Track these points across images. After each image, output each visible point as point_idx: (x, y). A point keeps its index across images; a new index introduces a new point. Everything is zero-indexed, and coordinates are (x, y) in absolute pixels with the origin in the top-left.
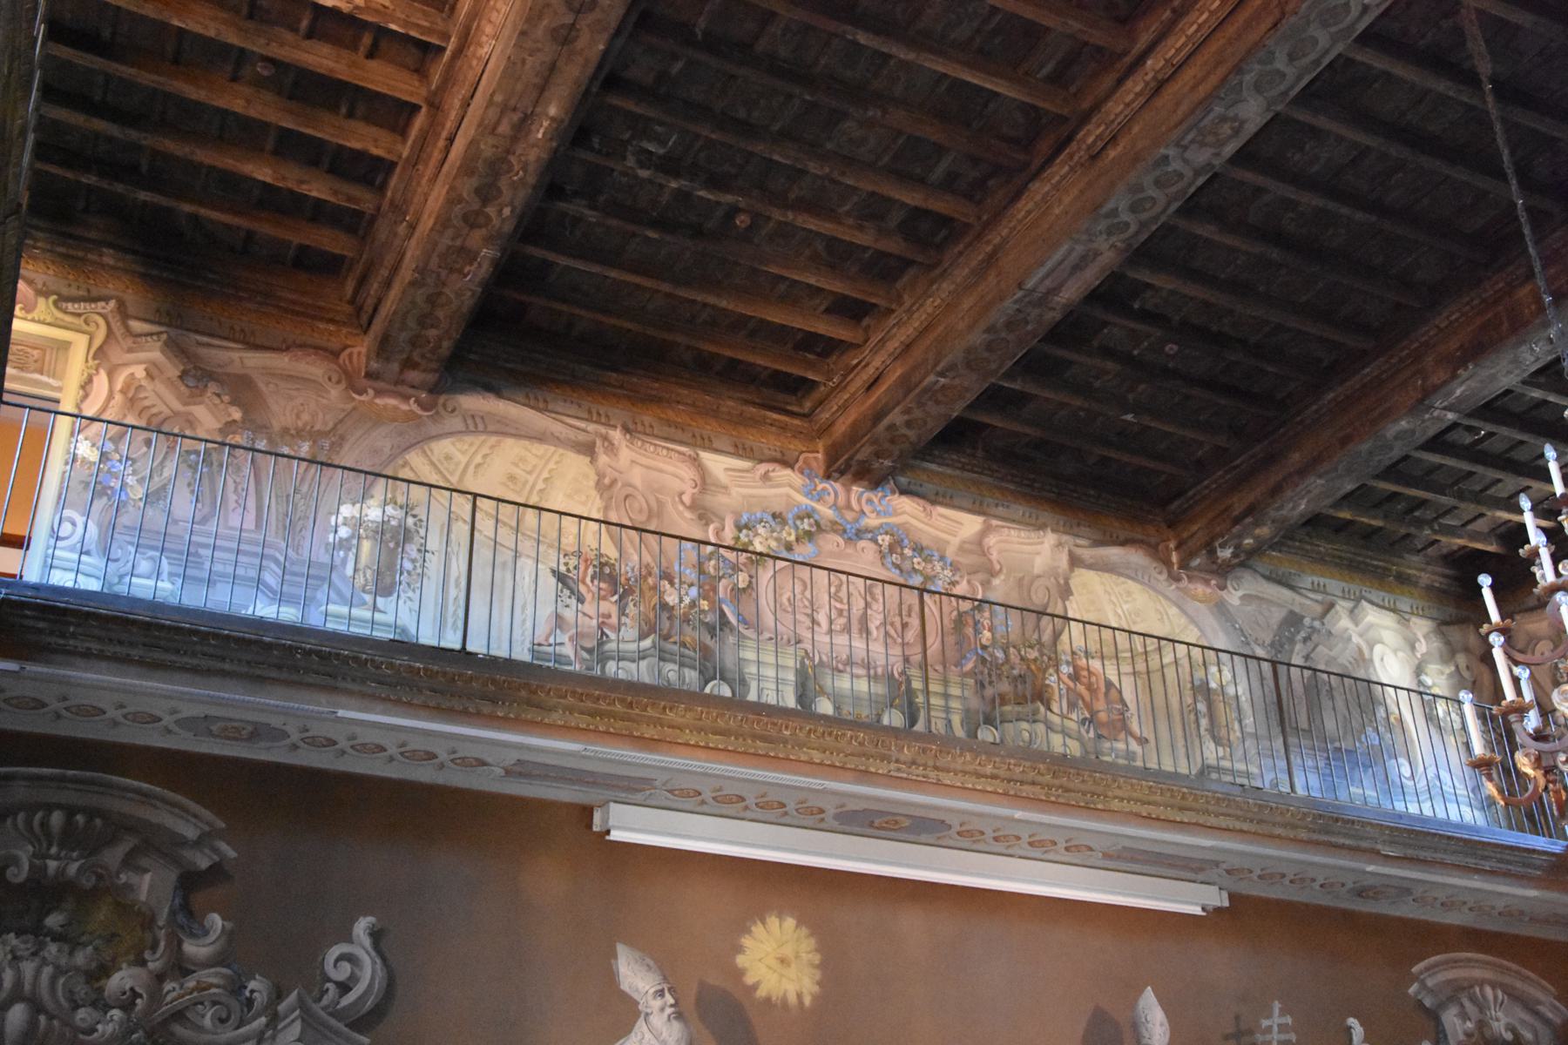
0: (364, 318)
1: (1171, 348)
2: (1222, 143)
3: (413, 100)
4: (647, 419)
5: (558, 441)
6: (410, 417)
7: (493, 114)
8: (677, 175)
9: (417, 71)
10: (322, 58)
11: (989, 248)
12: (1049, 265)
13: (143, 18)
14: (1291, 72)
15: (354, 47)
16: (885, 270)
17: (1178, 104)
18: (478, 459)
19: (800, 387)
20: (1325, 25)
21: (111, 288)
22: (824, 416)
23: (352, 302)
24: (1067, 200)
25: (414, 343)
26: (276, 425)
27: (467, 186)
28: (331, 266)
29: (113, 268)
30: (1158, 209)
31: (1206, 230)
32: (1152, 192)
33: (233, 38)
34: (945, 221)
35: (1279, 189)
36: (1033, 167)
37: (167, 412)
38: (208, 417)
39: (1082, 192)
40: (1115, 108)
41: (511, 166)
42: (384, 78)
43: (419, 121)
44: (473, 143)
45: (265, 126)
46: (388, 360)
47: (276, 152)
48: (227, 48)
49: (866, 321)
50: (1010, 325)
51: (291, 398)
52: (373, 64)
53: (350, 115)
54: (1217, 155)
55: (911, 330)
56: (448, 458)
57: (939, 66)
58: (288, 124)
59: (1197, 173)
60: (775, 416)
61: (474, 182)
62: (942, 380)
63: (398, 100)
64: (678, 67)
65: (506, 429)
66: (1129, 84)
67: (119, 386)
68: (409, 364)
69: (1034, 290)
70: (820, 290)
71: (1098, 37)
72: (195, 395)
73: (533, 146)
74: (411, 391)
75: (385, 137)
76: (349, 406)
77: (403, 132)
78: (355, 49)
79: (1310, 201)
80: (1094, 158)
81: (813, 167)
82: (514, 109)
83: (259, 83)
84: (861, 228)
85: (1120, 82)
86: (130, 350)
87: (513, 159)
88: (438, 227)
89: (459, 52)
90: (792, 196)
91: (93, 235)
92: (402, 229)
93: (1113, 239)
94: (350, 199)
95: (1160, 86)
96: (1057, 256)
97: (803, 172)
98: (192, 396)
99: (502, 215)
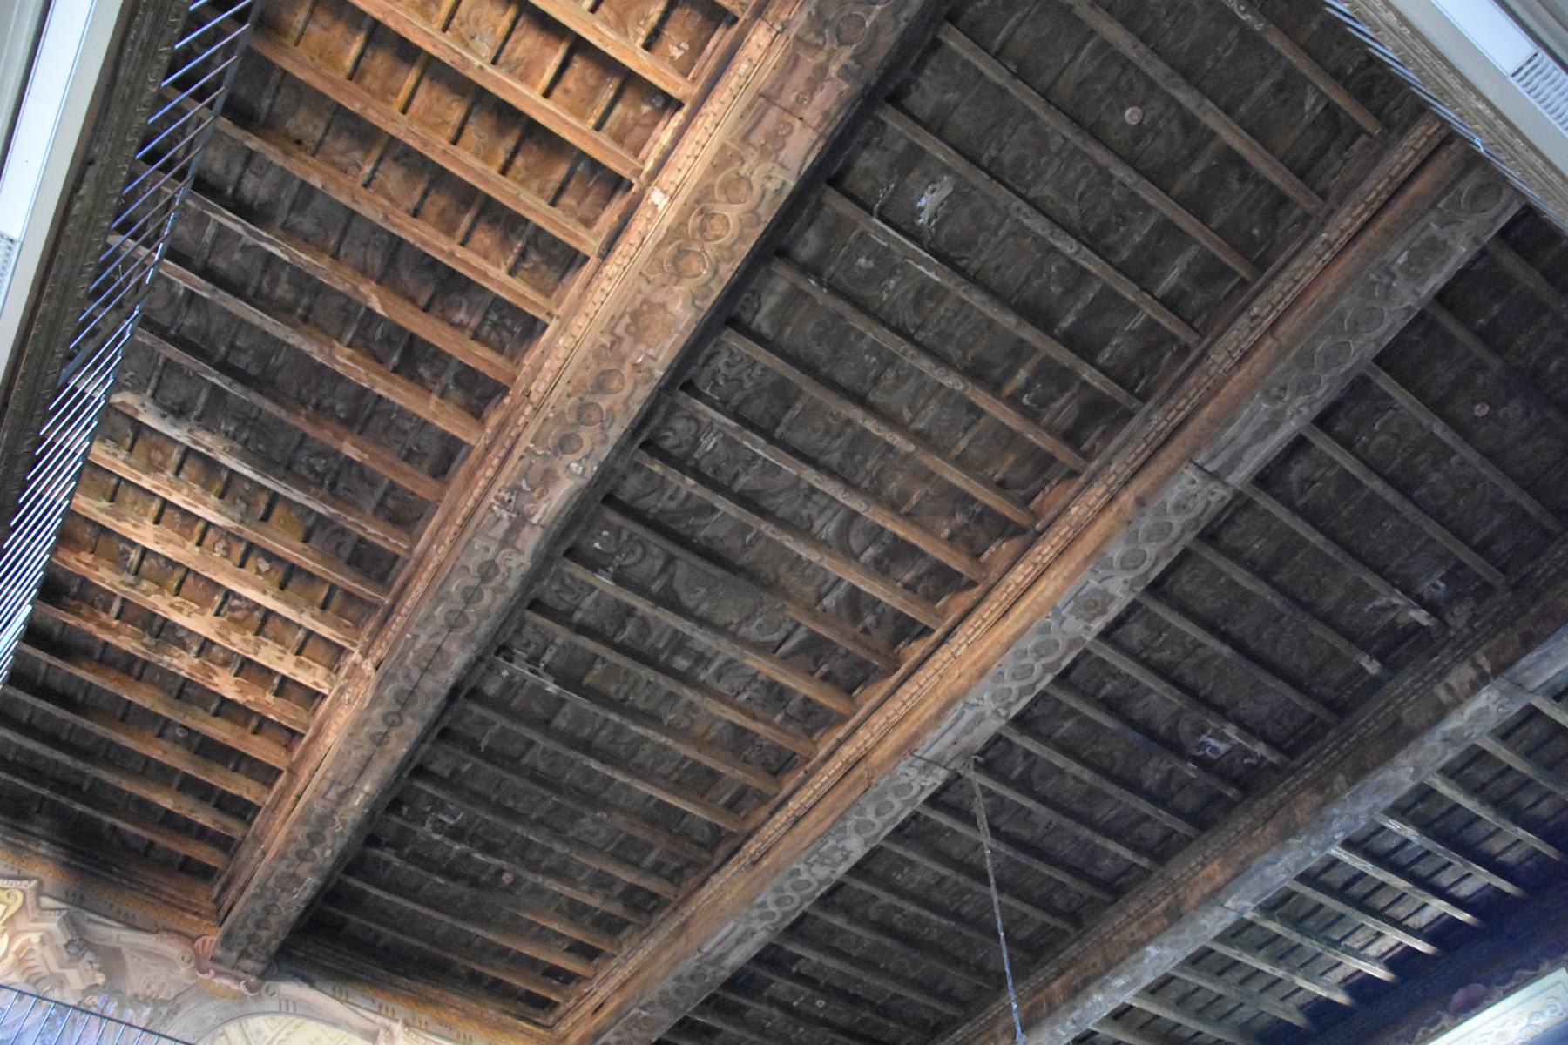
0: (222, 914)
1: (820, 1003)
2: (835, 865)
3: (279, 766)
4: (424, 1018)
5: (350, 1028)
6: (239, 997)
7: (324, 785)
10: (220, 731)
11: (683, 919)
13: (105, 691)
14: (878, 823)
15: (245, 724)
16: (611, 926)
18: (282, 1036)
19: (546, 1004)
20: (897, 794)
21: (38, 871)
22: (562, 1029)
23: (216, 901)
24: (735, 891)
25: (251, 938)
26: (129, 993)
27: (301, 833)
28: (206, 873)
29: (45, 856)
30: (795, 905)
31: (838, 921)
32: (789, 893)
33: (161, 710)
34: (654, 896)
35: (886, 898)
37: (45, 972)
38: (78, 979)
40: (768, 832)
42: (261, 749)
43: (281, 781)
45: (175, 771)
46: (229, 949)
47: (179, 789)
48: (156, 717)
49: (596, 961)
51: (147, 970)
52: (257, 738)
53: (235, 770)
56: (259, 1032)
58: (190, 771)
60: (525, 1025)
61: (307, 829)
62: (644, 1013)
64: (466, 768)
65: (310, 1013)
66: (777, 816)
67: (15, 947)
68: (244, 955)
69: (708, 954)
70: (563, 935)
71: (755, 783)
72: (74, 960)
74: (241, 974)
76: (192, 982)
77: (271, 786)
79: (912, 908)
80: (754, 863)
81: (558, 847)
83: (176, 741)
84: (591, 893)
85: (772, 814)
86: (35, 920)
87: (336, 818)
89: (314, 739)
90: (543, 865)
91: (36, 830)
92: (257, 854)
94: (225, 828)
95: (797, 821)
97: (551, 851)
98: (71, 961)
99: (326, 854)
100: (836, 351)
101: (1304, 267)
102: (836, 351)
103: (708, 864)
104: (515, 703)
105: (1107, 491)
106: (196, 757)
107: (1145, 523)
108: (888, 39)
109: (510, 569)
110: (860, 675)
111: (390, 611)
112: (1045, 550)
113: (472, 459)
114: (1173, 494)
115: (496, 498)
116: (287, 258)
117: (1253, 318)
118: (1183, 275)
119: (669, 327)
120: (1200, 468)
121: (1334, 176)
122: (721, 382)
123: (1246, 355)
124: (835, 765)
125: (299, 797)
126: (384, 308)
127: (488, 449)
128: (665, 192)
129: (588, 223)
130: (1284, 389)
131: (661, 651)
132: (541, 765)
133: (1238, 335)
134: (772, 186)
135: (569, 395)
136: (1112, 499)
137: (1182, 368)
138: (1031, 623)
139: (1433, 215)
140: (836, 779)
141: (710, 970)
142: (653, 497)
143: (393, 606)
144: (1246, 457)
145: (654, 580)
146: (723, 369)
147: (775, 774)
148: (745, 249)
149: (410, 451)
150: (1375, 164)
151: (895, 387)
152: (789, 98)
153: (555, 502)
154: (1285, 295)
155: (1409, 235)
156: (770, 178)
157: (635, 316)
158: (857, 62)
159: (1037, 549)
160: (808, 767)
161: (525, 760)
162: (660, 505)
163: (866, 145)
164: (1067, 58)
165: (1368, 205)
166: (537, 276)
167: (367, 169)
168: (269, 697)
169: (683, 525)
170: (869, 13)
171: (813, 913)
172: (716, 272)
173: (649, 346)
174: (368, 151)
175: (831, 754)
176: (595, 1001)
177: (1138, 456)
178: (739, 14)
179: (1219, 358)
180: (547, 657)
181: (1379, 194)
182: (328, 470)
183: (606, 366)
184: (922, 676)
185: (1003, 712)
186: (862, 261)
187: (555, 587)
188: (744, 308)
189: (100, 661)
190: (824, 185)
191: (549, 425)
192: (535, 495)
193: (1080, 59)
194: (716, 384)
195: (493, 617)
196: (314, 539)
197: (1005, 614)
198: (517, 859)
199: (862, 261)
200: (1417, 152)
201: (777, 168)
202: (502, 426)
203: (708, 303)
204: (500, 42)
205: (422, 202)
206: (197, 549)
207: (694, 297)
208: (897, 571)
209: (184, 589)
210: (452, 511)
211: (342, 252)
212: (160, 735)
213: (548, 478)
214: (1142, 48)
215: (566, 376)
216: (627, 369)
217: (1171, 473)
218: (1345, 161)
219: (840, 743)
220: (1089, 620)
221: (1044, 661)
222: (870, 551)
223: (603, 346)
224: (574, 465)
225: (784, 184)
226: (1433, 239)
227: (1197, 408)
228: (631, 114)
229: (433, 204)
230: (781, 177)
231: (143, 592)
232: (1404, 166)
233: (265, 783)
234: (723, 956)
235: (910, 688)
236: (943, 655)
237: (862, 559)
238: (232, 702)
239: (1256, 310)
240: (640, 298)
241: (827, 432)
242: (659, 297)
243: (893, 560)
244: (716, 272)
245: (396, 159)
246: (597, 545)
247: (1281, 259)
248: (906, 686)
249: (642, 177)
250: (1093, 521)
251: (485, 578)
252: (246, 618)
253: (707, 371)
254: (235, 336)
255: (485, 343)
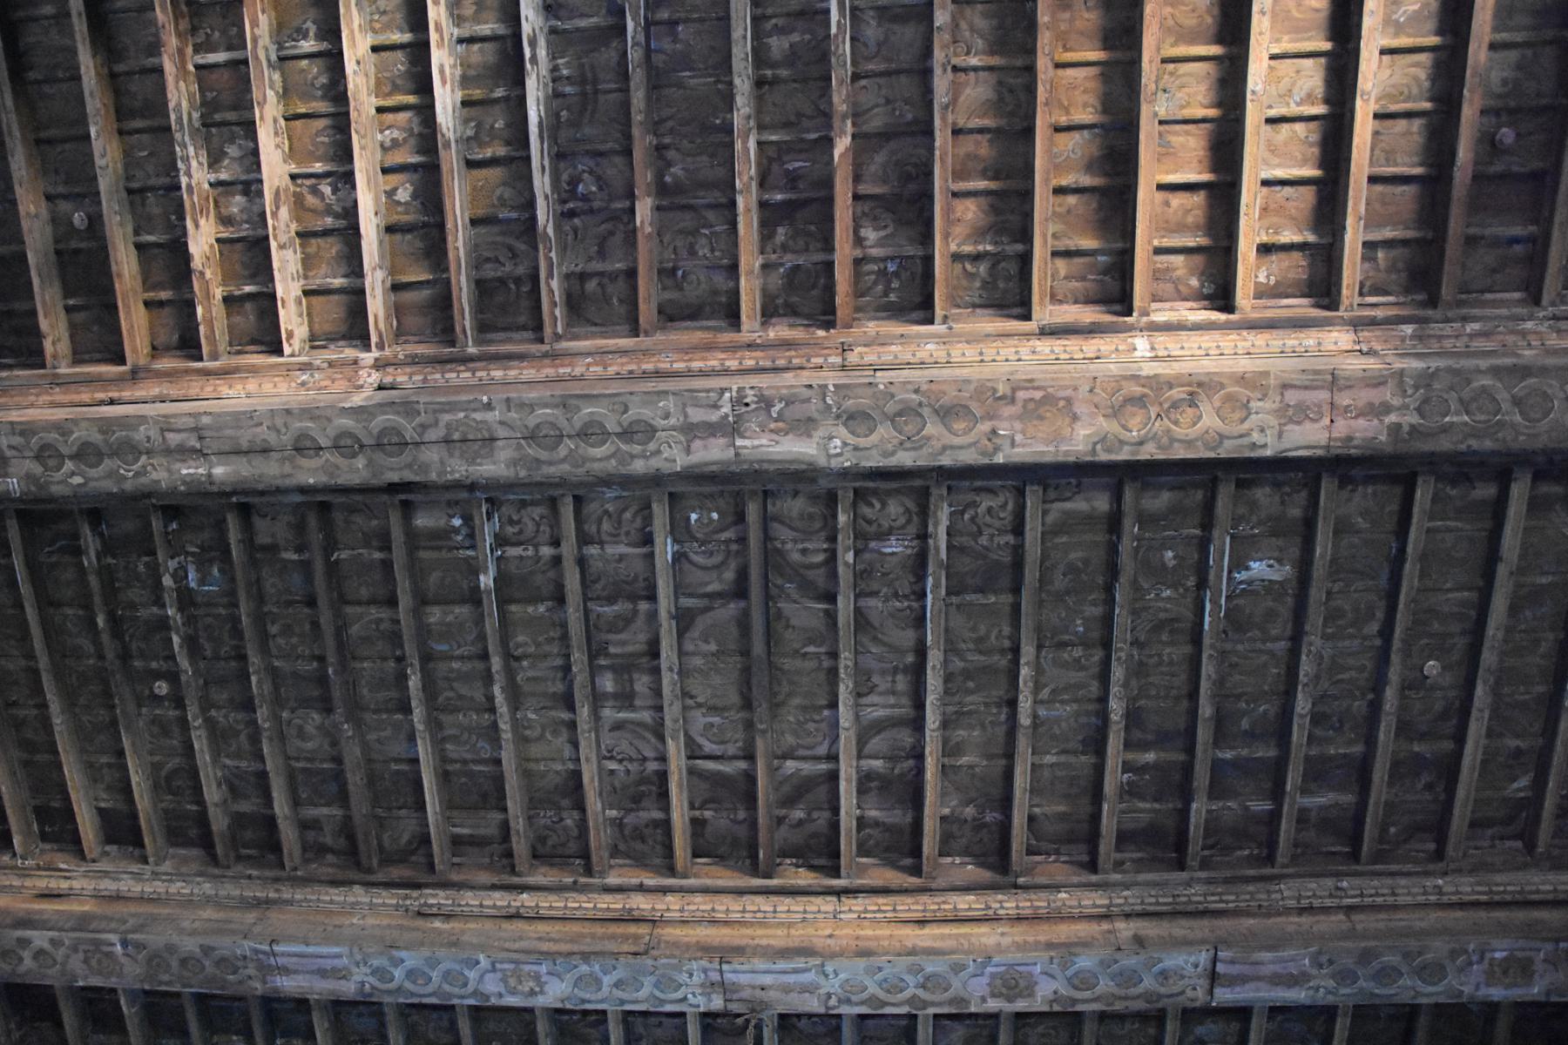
2: (513, 992)
8: (181, 609)
9: (154, 348)
10: (125, 264)
11: (272, 895)
12: (311, 950)
17: (521, 938)
24: (371, 921)
33: (104, 184)
34: (275, 847)
36: (372, 878)
39: (389, 926)
40: (470, 899)
41: (137, 460)
44: (143, 419)
50: (221, 962)
53: (68, 310)
54: (500, 995)
55: (139, 889)
57: (423, 750)
58: (32, 258)
59: (475, 993)
61: (96, 437)
63: (121, 344)
66: (497, 894)
73: (169, 471)
75: (64, 347)
78: (146, 290)
82: (201, 438)
85: (494, 887)
87: (144, 458)
88: (18, 428)
89: (207, 373)
90: (213, 713)
93: (371, 979)
96: (324, 950)
100: (1068, 592)
101: (1409, 889)
102: (1068, 592)
103: (370, 871)
104: (423, 554)
105: (1108, 907)
106: (53, 257)
107: (1129, 961)
108: (1445, 444)
109: (658, 452)
110: (722, 850)
111: (466, 360)
112: (1008, 903)
113: (727, 337)
114: (1173, 960)
115: (740, 390)
116: (834, 30)
117: (1338, 888)
118: (1321, 808)
119: (1057, 438)
120: (1215, 960)
121: (1476, 848)
122: (967, 516)
123: (1310, 910)
124: (615, 903)
125: (112, 402)
126: (841, 156)
127: (751, 346)
128: (1153, 349)
129: (1055, 299)
130: (1331, 962)
131: (607, 655)
132: (355, 630)
133: (1316, 889)
134: (1256, 437)
135: (916, 391)
136: (1106, 917)
137: (1252, 872)
138: (952, 952)
139: (1549, 946)
140: (600, 915)
141: (251, 971)
142: (790, 534)
143: (471, 359)
144: (1251, 985)
145: (691, 595)
146: (982, 509)
147: (535, 856)
148: (1180, 453)
149: (674, 270)
150: (1518, 869)
151: (1065, 665)
152: (1344, 399)
153: (778, 449)
154: (1377, 895)
155: (1521, 943)
156: (1262, 431)
157: (1048, 400)
158: (1410, 433)
159: (1000, 897)
160: (583, 880)
161: (349, 610)
162: (789, 546)
163: (1277, 485)
164: (1448, 585)
165: (1491, 892)
166: (964, 283)
167: (974, 61)
168: (218, 293)
169: (779, 582)
170: (1457, 413)
171: (386, 1009)
172: (1141, 443)
173: (1023, 432)
174: (992, 53)
175: (619, 889)
176: (57, 884)
177: (1158, 903)
178: (1342, 308)
179: (1287, 892)
180: (513, 552)
181: (1504, 892)
182: (585, 198)
183: (974, 407)
184: (785, 903)
185: (833, 1002)
186: (1170, 554)
187: (610, 507)
188: (1056, 488)
189: (113, 76)
190: (1233, 477)
191: (869, 391)
192: (773, 426)
193: (1450, 595)
194: (962, 513)
195: (581, 471)
196: (482, 230)
197: (921, 923)
198: (201, 681)
199: (1170, 554)
200: (1555, 890)
201: (1276, 431)
202: (787, 344)
203: (1103, 457)
204: (1179, 117)
205: (971, 131)
206: (373, 111)
207: (1103, 440)
208: (872, 799)
209: (298, 123)
210: (646, 352)
211: (863, 82)
212: (49, 198)
213: (804, 426)
214: (1500, 635)
215: (934, 373)
216: (985, 427)
217: (1186, 943)
218: (1493, 846)
219: (641, 888)
220: (993, 995)
221: (920, 992)
222: (877, 764)
223: (995, 390)
224: (838, 442)
225: (1265, 446)
226: (1530, 961)
227: (1247, 913)
228: (1179, 273)
229: (978, 143)
230: (1269, 440)
231: (270, 79)
232: (1538, 892)
233: (75, 352)
234: (285, 971)
235: (764, 904)
236: (827, 904)
237: (863, 762)
238: (186, 257)
239: (1345, 884)
240: (1068, 393)
241: (980, 640)
242: (1080, 408)
243: (880, 789)
244: (1141, 443)
245: (1000, 83)
246: (694, 517)
247: (1394, 867)
248: (759, 899)
249: (1145, 319)
250: (1072, 918)
251: (627, 434)
252: (313, 211)
253: (971, 497)
254: (686, 21)
255: (857, 275)
